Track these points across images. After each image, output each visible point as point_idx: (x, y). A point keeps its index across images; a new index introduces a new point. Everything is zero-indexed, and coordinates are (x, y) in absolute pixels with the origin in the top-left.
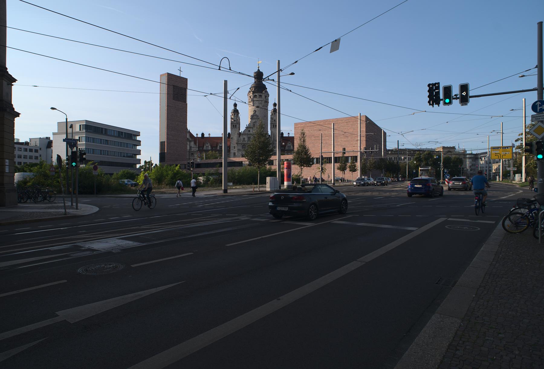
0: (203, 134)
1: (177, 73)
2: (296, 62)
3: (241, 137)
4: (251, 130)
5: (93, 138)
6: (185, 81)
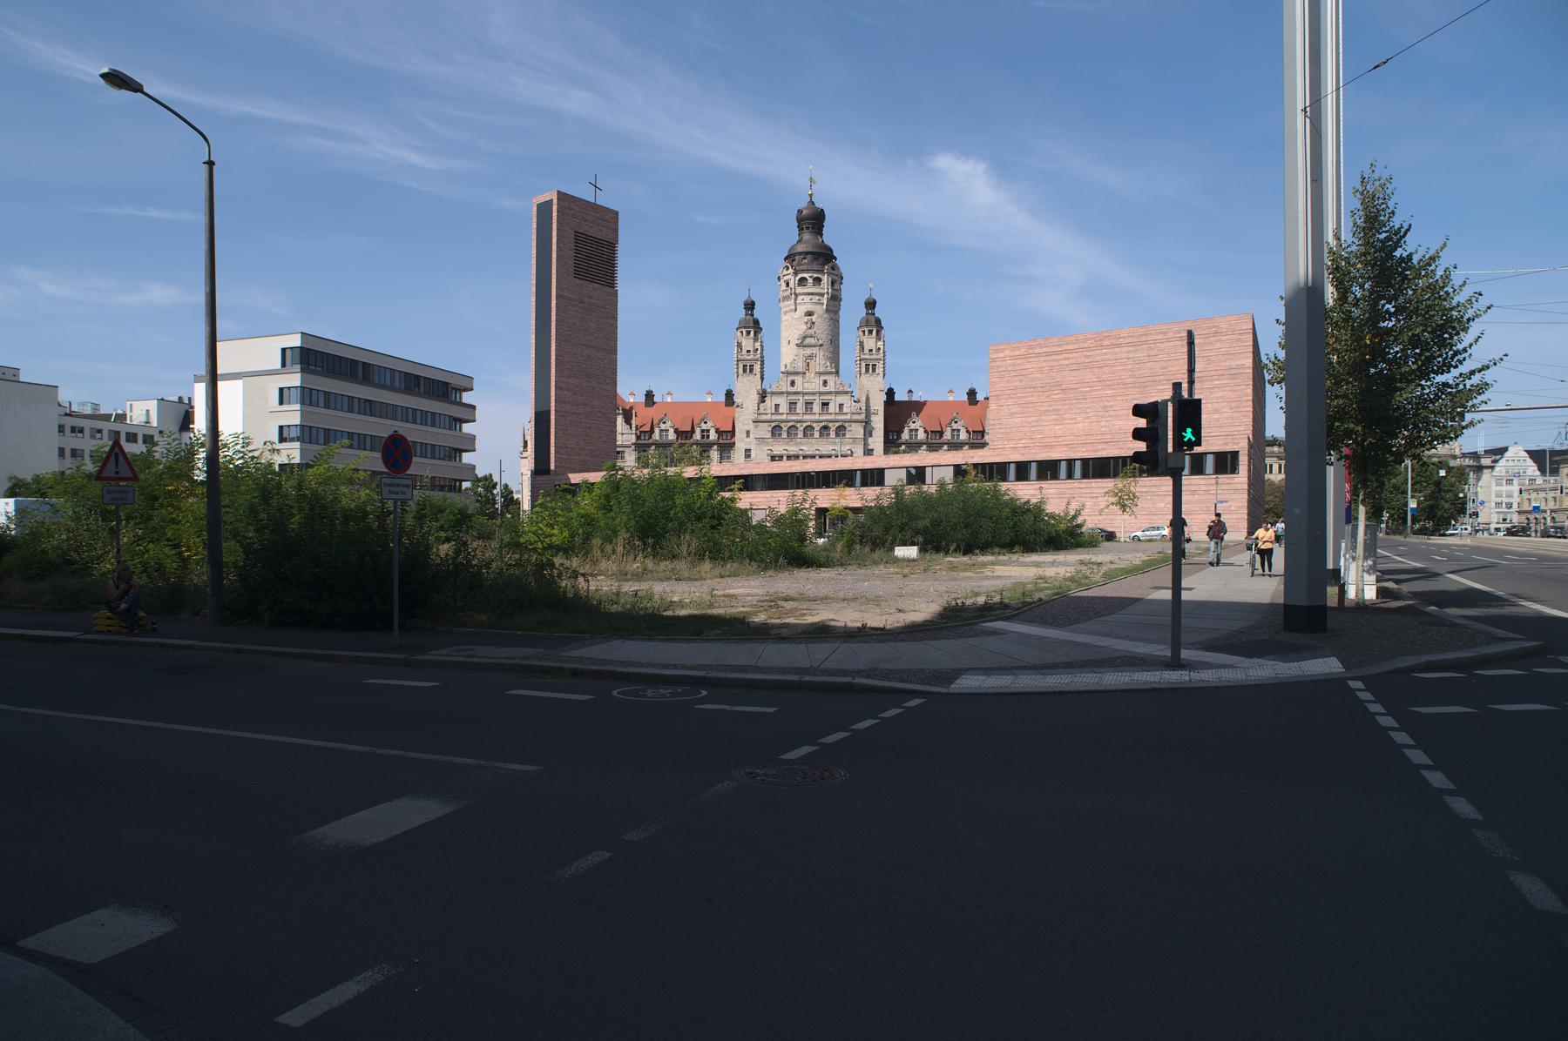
1: (587, 194)
4: (798, 380)
6: (610, 218)
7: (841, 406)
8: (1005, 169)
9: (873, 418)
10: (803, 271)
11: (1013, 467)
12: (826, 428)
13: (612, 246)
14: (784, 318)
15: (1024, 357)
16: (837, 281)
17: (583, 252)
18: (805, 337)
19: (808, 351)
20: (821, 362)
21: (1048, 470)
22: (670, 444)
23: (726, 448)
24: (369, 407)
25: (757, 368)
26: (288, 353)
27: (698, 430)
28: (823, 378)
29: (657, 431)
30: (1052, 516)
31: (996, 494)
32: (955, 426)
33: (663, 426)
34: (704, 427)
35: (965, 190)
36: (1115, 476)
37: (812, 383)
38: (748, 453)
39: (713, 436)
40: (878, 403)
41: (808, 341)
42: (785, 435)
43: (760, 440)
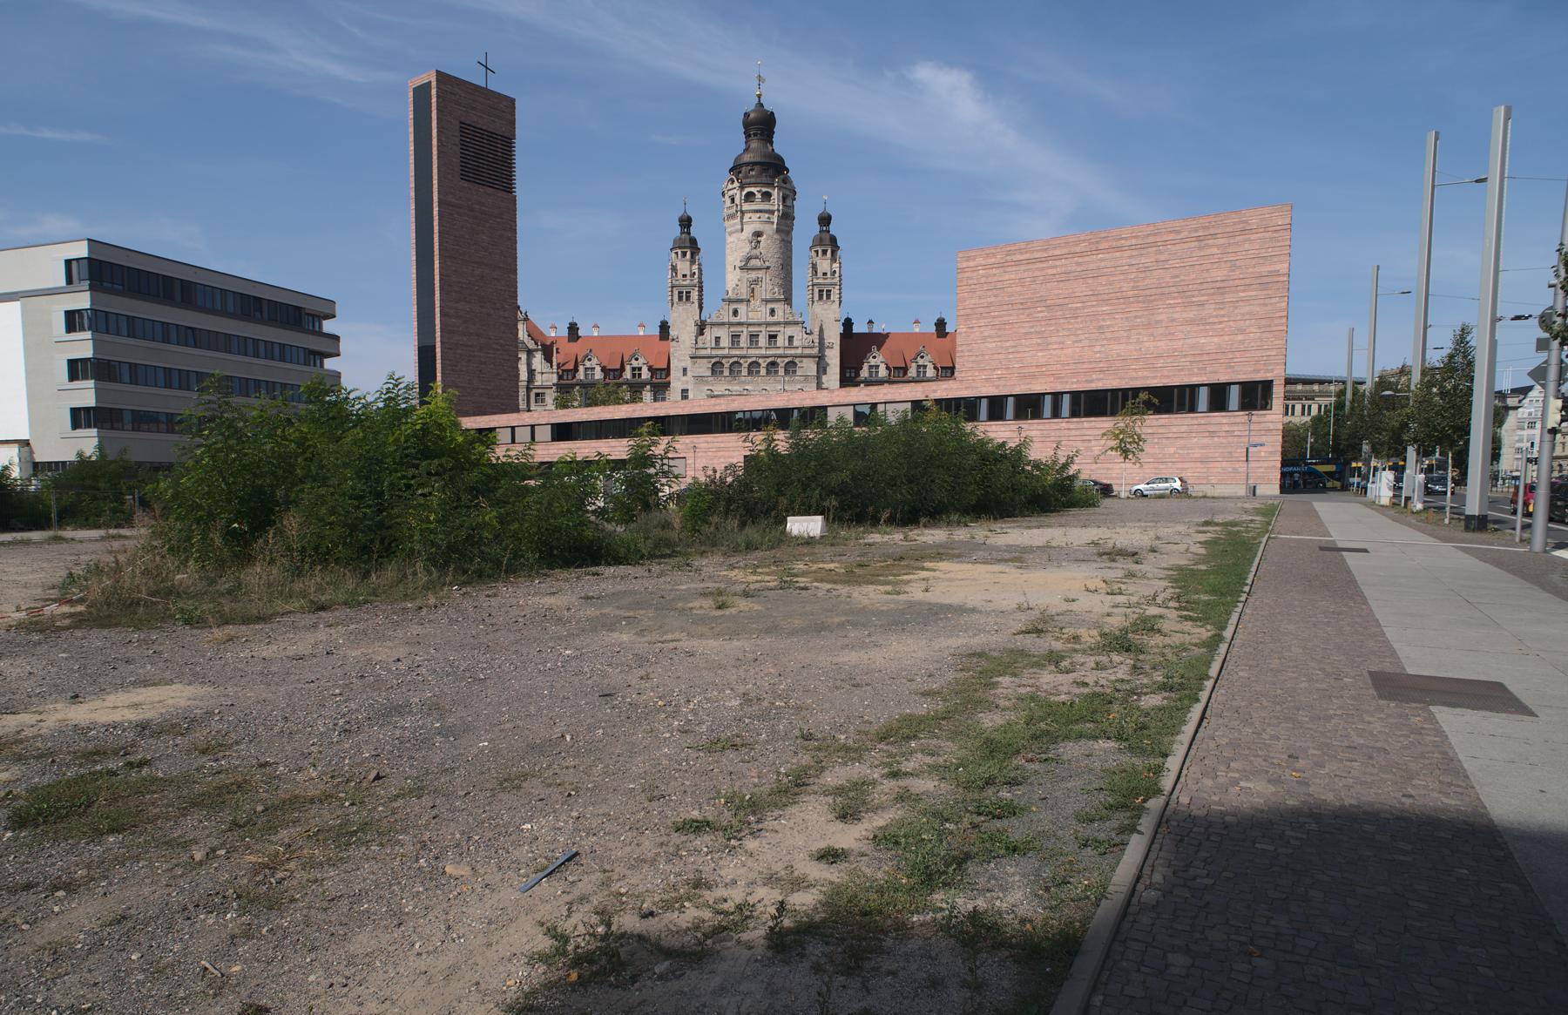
0: (76, 369)
2: (1518, 318)
3: (707, 331)
4: (742, 308)
5: (131, 320)
7: (791, 338)
8: (990, 80)
9: (827, 352)
10: (750, 185)
11: (984, 403)
12: (773, 364)
13: (507, 142)
14: (730, 239)
15: (1001, 266)
16: (789, 195)
17: (471, 147)
18: (749, 258)
19: (753, 275)
20: (769, 286)
21: (1029, 406)
22: (593, 385)
23: (661, 390)
24: (193, 337)
25: (695, 295)
26: (74, 265)
27: (628, 368)
28: (770, 306)
29: (581, 369)
30: (1037, 465)
31: (960, 436)
32: (921, 361)
33: (588, 364)
34: (635, 364)
35: (949, 103)
36: (1113, 414)
37: (759, 313)
38: (685, 394)
39: (645, 374)
40: (833, 335)
41: (753, 263)
42: (726, 373)
43: (699, 379)
